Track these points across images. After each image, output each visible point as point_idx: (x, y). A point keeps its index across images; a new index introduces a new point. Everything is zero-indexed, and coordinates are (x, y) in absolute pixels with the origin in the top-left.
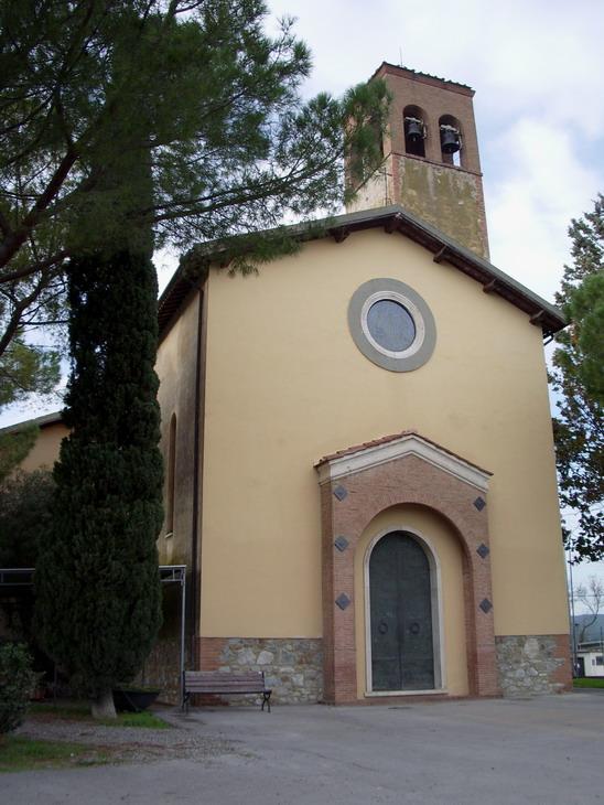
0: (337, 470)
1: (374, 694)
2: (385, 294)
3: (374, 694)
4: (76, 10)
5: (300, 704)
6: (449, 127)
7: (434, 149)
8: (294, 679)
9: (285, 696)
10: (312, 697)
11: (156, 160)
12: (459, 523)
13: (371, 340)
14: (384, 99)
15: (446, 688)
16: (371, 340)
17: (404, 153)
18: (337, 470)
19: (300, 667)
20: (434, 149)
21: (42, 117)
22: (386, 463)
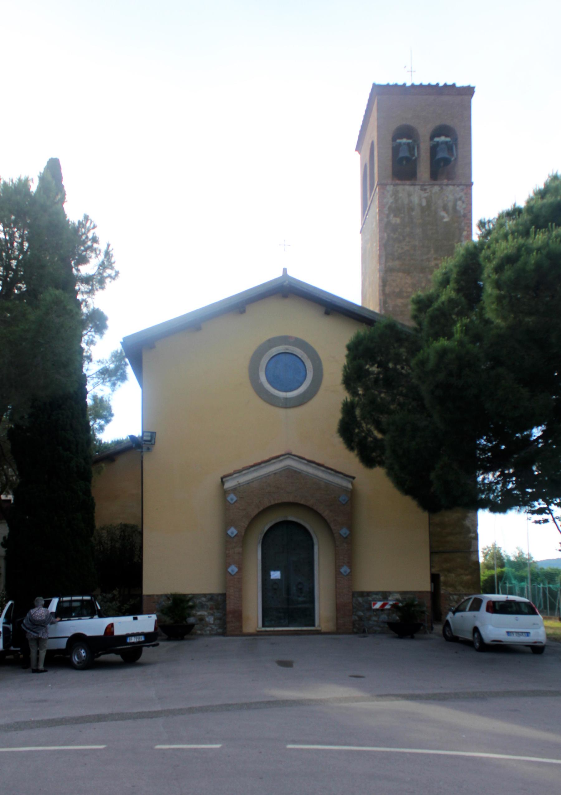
0: (229, 485)
1: (264, 629)
2: (281, 348)
3: (264, 629)
4: (14, 215)
5: (211, 635)
6: (443, 139)
7: (424, 170)
8: (207, 619)
9: (200, 630)
10: (219, 631)
11: (483, 230)
12: (326, 514)
13: (282, 394)
14: (89, 222)
15: (319, 626)
16: (282, 394)
17: (390, 181)
18: (229, 485)
19: (211, 612)
20: (424, 170)
21: (488, 440)
22: (268, 476)
